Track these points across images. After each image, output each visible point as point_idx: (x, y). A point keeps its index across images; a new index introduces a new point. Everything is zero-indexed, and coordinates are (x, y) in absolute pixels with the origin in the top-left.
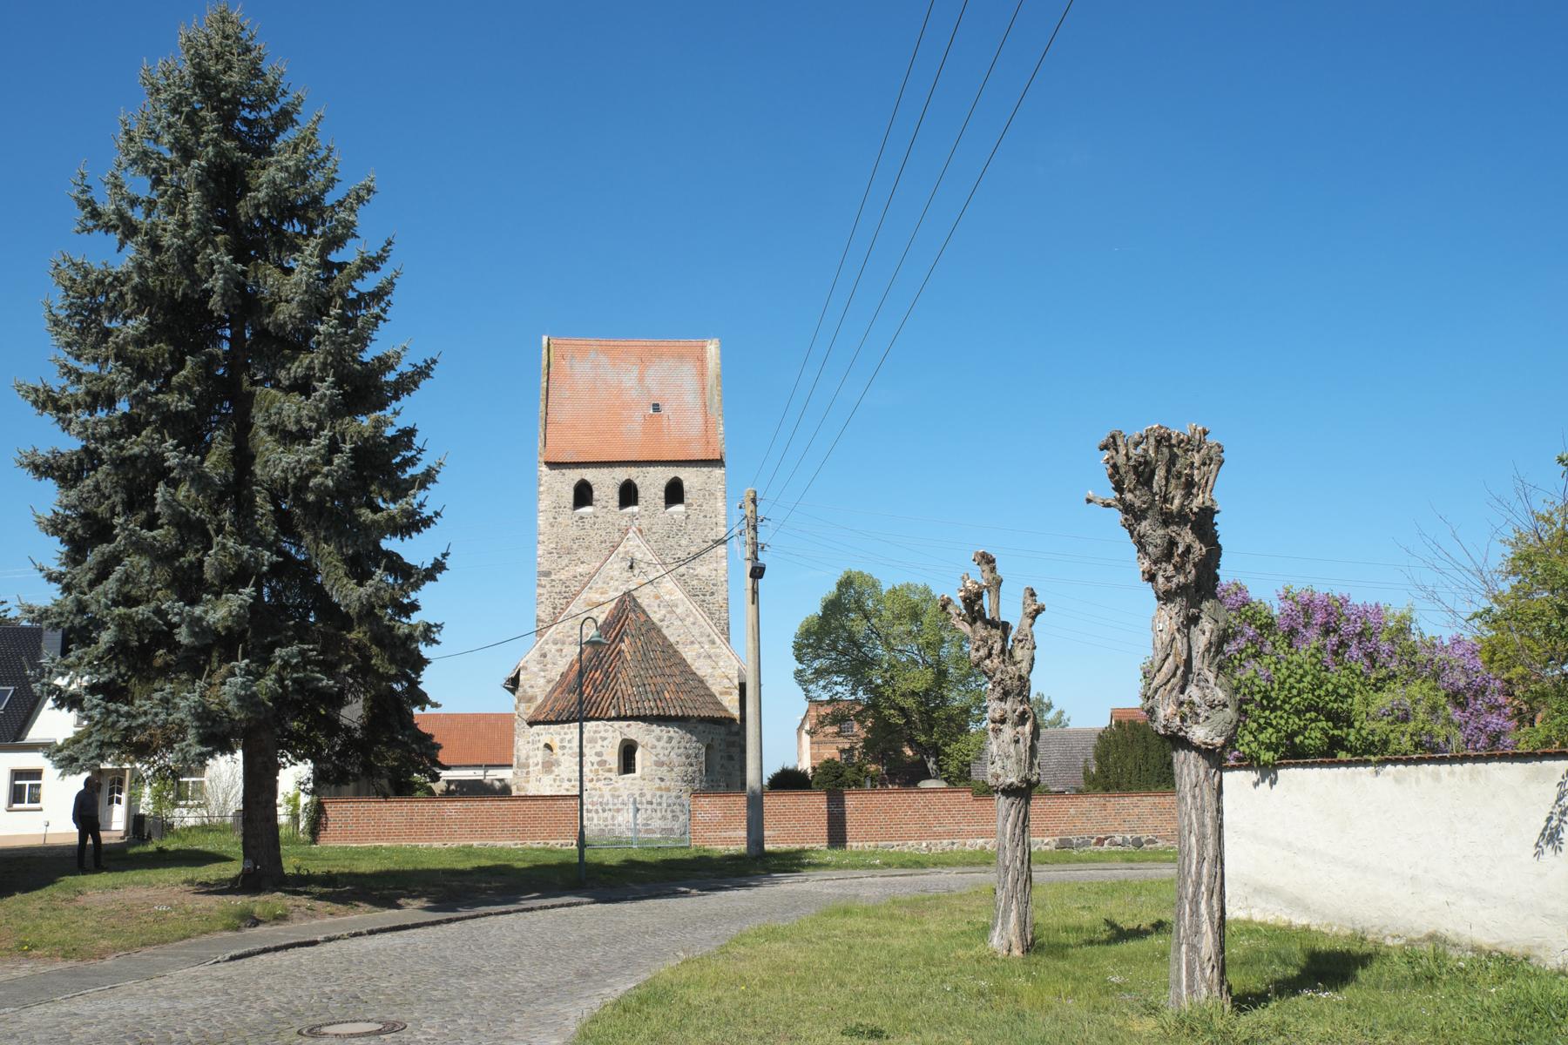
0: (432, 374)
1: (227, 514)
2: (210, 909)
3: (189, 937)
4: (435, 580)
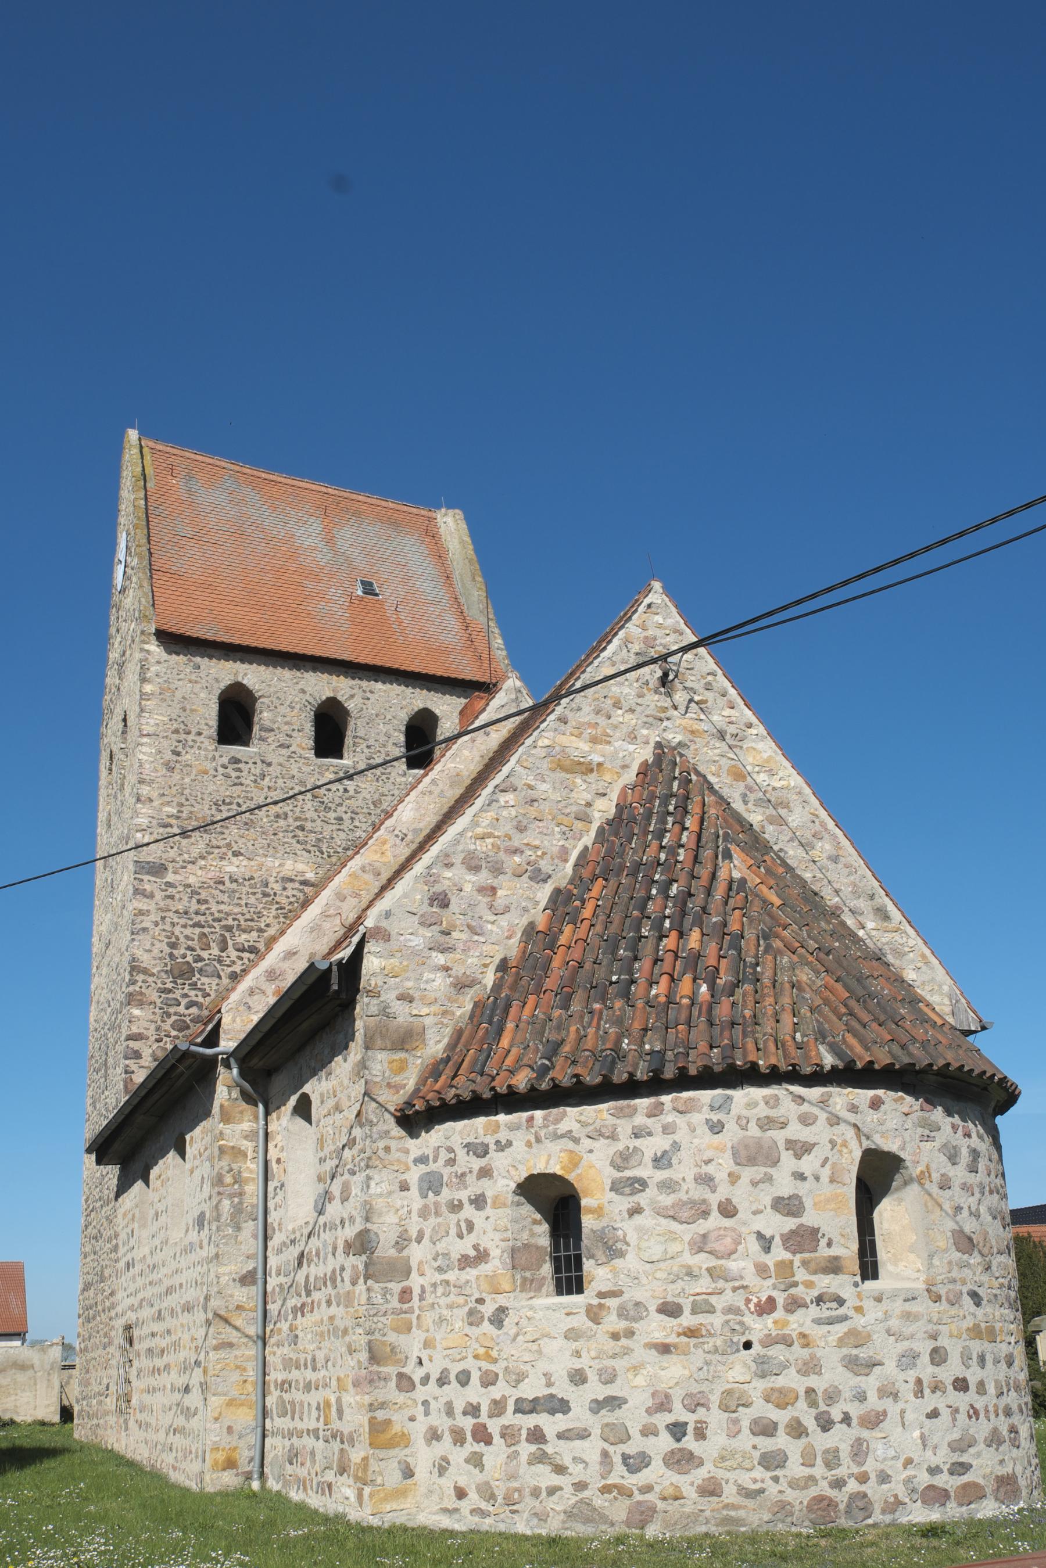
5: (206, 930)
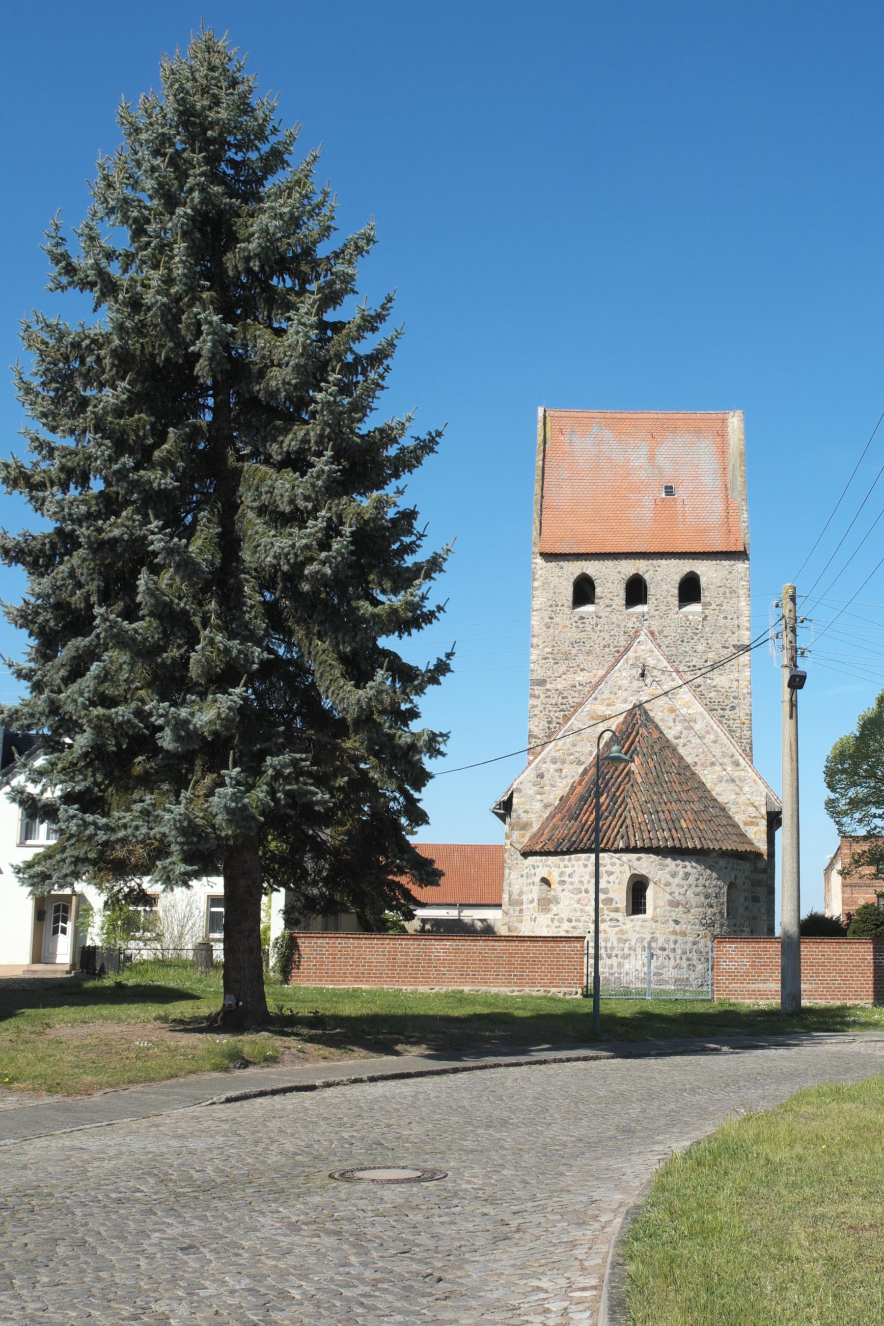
0: (436, 448)
1: (213, 605)
2: (195, 1048)
3: (177, 1076)
4: (439, 683)
5: (566, 713)
